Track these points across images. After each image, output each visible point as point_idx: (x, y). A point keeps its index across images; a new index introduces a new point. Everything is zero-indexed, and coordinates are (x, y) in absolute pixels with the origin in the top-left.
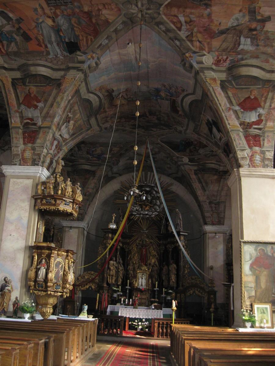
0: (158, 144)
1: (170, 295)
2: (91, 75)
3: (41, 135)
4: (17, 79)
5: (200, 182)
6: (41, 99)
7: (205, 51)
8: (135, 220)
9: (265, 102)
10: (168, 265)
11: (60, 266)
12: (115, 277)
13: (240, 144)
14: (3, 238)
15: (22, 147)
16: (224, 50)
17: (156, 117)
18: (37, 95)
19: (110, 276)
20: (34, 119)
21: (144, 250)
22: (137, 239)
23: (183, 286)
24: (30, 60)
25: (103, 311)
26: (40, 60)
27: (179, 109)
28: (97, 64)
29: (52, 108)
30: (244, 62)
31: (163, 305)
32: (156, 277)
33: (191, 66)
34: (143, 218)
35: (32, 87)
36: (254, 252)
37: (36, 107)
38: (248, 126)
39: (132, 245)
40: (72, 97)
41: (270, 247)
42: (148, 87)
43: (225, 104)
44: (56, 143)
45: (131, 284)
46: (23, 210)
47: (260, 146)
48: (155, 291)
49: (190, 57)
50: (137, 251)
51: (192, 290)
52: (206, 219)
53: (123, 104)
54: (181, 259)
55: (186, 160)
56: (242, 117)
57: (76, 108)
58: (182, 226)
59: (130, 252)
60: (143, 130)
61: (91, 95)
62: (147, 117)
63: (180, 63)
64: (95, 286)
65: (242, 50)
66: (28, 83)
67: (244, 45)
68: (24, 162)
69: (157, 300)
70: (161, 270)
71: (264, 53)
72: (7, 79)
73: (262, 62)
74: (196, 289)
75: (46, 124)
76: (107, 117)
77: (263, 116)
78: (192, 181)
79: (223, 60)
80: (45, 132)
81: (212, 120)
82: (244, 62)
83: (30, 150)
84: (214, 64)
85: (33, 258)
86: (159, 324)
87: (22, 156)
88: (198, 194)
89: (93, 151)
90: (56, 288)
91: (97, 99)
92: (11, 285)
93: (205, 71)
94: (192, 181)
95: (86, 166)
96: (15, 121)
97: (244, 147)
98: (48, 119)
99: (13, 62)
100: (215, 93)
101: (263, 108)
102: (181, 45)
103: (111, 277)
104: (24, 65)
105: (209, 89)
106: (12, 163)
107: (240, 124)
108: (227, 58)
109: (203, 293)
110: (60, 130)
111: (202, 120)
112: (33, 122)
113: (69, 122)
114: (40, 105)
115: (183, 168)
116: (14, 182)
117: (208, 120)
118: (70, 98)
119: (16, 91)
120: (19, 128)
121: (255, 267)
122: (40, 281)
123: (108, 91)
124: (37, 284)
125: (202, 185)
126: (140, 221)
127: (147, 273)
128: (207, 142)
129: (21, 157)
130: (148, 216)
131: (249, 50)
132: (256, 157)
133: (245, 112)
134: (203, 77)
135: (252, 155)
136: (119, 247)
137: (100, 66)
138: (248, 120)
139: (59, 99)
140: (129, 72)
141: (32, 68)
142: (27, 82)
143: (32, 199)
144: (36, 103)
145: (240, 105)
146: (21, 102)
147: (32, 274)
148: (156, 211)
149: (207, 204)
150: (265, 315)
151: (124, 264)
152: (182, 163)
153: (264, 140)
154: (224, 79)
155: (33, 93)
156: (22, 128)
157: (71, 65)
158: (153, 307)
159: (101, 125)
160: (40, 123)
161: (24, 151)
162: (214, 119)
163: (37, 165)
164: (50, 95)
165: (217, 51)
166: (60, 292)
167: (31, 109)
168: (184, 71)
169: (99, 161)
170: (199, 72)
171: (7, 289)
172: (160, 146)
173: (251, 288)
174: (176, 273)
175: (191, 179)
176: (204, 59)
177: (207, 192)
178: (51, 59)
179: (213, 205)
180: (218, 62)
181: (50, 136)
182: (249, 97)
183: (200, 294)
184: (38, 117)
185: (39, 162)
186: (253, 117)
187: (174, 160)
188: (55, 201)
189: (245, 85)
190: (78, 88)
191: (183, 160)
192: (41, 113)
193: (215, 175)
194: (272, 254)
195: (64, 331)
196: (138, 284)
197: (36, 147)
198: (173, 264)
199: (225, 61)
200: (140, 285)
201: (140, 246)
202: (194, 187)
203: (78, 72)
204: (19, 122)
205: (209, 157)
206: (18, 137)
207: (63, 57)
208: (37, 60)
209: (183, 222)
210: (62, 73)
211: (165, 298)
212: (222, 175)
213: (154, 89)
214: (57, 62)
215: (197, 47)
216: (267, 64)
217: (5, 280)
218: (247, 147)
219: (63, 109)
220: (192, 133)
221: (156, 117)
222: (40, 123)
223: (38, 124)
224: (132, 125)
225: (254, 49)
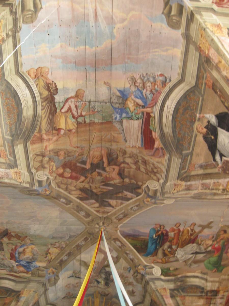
0: (116, 239)
2: (50, 288)
17: (117, 168)
42: (110, 88)
53: (70, 131)
55: (157, 271)
63: (163, 13)
84: (216, 3)
89: (19, 253)
95: (7, 282)
100: (223, 45)
105: (212, 40)
115: (153, 287)
134: (201, 20)
140: (82, 47)
152: (152, 277)
159: (33, 171)
169: (27, 273)
170: (194, 13)
172: (120, 244)
187: (140, 273)
191: (154, 271)
193: (200, 297)
203: (4, 8)
205: (191, 265)
212: (211, 299)
220: (175, 185)
221: (117, 168)
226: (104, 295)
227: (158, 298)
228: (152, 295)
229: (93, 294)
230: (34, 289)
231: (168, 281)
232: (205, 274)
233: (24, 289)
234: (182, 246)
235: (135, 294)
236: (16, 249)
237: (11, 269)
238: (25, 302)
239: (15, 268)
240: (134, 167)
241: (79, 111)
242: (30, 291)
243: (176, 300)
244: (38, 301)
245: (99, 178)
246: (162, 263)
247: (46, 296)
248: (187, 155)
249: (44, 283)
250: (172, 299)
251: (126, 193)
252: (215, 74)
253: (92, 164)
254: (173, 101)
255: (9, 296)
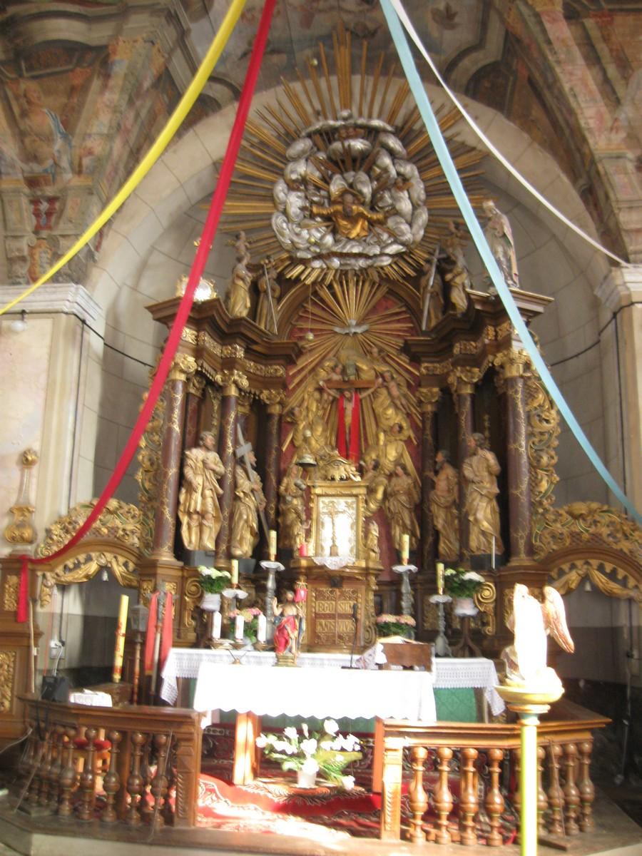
1: (470, 596)
2: (193, 26)
5: (593, 59)
8: (308, 282)
10: (456, 461)
12: (216, 518)
19: (189, 514)
21: (349, 407)
22: (320, 364)
23: (531, 551)
25: (150, 677)
31: (441, 642)
32: (408, 522)
34: (343, 274)
39: (299, 391)
45: (285, 554)
48: (400, 575)
50: (320, 413)
51: (573, 567)
52: (626, 239)
54: (517, 426)
58: (515, 270)
59: (287, 422)
64: (126, 565)
69: (408, 619)
70: (426, 486)
74: (595, 563)
78: (552, 50)
86: (409, 756)
88: (582, 122)
94: (552, 50)
95: (62, 23)
103: (194, 524)
109: (632, 582)
125: (604, 71)
126: (330, 287)
127: (356, 496)
130: (362, 263)
136: (233, 392)
148: (396, 242)
149: (630, 167)
151: (261, 468)
158: (382, 659)
174: (496, 490)
175: (549, 42)
177: (627, 112)
183: (615, 587)
195: (184, 720)
196: (319, 548)
198: (480, 452)
200: (327, 551)
201: (332, 392)
202: (567, 87)
209: (517, 252)
211: (449, 608)
226: (365, 37)
227: (524, 21)
228: (505, 16)
229: (330, 36)
230: (145, 35)
233: (115, 37)
235: (457, 20)
238: (126, 75)
242: (135, 41)
243: (584, 28)
244: (167, 69)
247: (189, 54)
249: (170, 12)
250: (569, 25)
255: (78, 64)
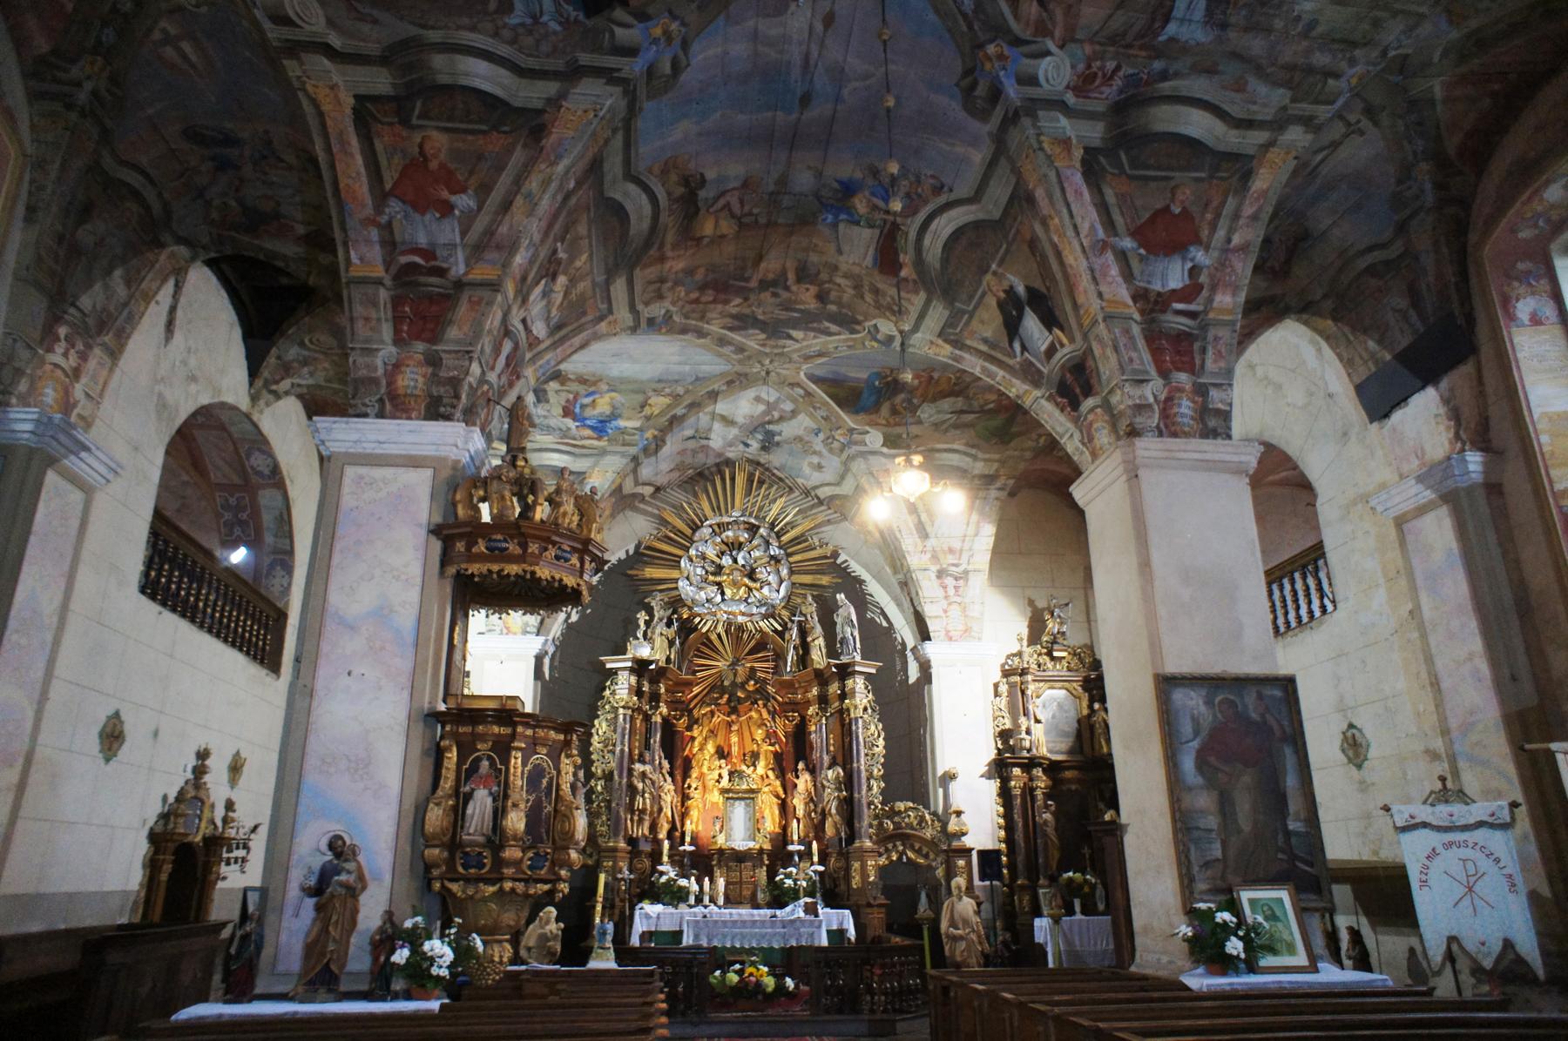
0: (798, 385)
3: (463, 309)
4: (376, 99)
6: (467, 180)
7: (1053, 38)
9: (1213, 227)
11: (545, 781)
13: (1131, 360)
14: (319, 684)
15: (387, 351)
16: (1113, 40)
17: (813, 290)
18: (452, 166)
19: (633, 813)
20: (438, 253)
24: (433, 28)
26: (473, 29)
27: (906, 258)
28: (676, 68)
29: (507, 218)
30: (1166, 87)
33: (996, 94)
35: (435, 134)
36: (1203, 708)
37: (446, 209)
38: (1156, 302)
40: (579, 184)
41: (1254, 695)
42: (819, 174)
43: (1092, 227)
44: (507, 347)
46: (397, 578)
47: (1191, 371)
49: (1001, 57)
53: (723, 237)
56: (1142, 272)
57: (582, 229)
60: (763, 336)
61: (632, 188)
62: (787, 288)
63: (957, 85)
65: (1172, 40)
66: (419, 117)
67: (1182, 21)
68: (394, 405)
71: (1236, 56)
72: (336, 96)
73: (1224, 87)
75: (481, 272)
76: (662, 281)
77: (1205, 271)
79: (1104, 75)
80: (479, 303)
81: (1028, 288)
82: (1166, 87)
83: (420, 364)
85: (439, 755)
87: (389, 384)
89: (583, 407)
90: (530, 867)
91: (647, 209)
92: (359, 868)
93: (1041, 113)
95: (556, 456)
96: (364, 257)
97: (1147, 372)
98: (491, 255)
99: (366, 28)
100: (1063, 190)
101: (1207, 248)
102: (975, 11)
104: (406, 44)
106: (351, 411)
107: (1135, 298)
108: (1118, 68)
109: (932, 856)
110: (525, 301)
111: (984, 294)
112: (433, 263)
113: (554, 277)
114: (464, 201)
116: (361, 477)
117: (1010, 291)
118: (572, 185)
119: (372, 144)
120: (379, 282)
121: (1212, 759)
122: (473, 844)
123: (686, 181)
124: (458, 855)
128: (984, 369)
129: (383, 390)
131: (1192, 43)
132: (1180, 406)
133: (1152, 257)
135: (1169, 399)
137: (683, 77)
138: (1157, 286)
139: (533, 184)
140: (770, 114)
141: (438, 60)
142: (417, 112)
143: (433, 539)
144: (445, 194)
145: (1135, 234)
146: (388, 186)
147: (436, 817)
150: (1280, 925)
153: (1204, 351)
154: (1097, 143)
155: (435, 156)
156: (388, 282)
157: (585, 59)
160: (459, 268)
161: (397, 366)
162: (1038, 284)
163: (448, 418)
164: (500, 169)
165: (1091, 41)
166: (545, 882)
167: (428, 217)
168: (962, 115)
169: (599, 438)
171: (341, 884)
172: (801, 392)
173: (1210, 831)
176: (1045, 67)
178: (514, 28)
179: (950, 581)
180: (1084, 84)
181: (493, 320)
182: (1167, 209)
184: (455, 246)
185: (454, 407)
186: (1174, 276)
188: (524, 546)
189: (1159, 168)
190: (601, 151)
192: (463, 234)
194: (1262, 716)
197: (443, 356)
199: (1108, 79)
203: (610, 89)
204: (379, 259)
206: (374, 315)
207: (560, 23)
208: (459, 28)
210: (551, 88)
213: (836, 185)
214: (538, 42)
215: (1027, 24)
216: (1238, 97)
217: (331, 846)
218: (1153, 373)
219: (544, 224)
221: (813, 290)
222: (462, 269)
223: (453, 272)
224: (733, 317)
225: (1211, 38)
231: (922, 316)
232: (973, 446)
234: (934, 400)
236: (575, 399)
237: (565, 433)
239: (574, 431)
240: (851, 291)
241: (747, 208)
245: (772, 300)
246: (888, 425)
248: (964, 312)
251: (827, 324)
252: (1038, 228)
253: (761, 282)
254: (950, 221)
